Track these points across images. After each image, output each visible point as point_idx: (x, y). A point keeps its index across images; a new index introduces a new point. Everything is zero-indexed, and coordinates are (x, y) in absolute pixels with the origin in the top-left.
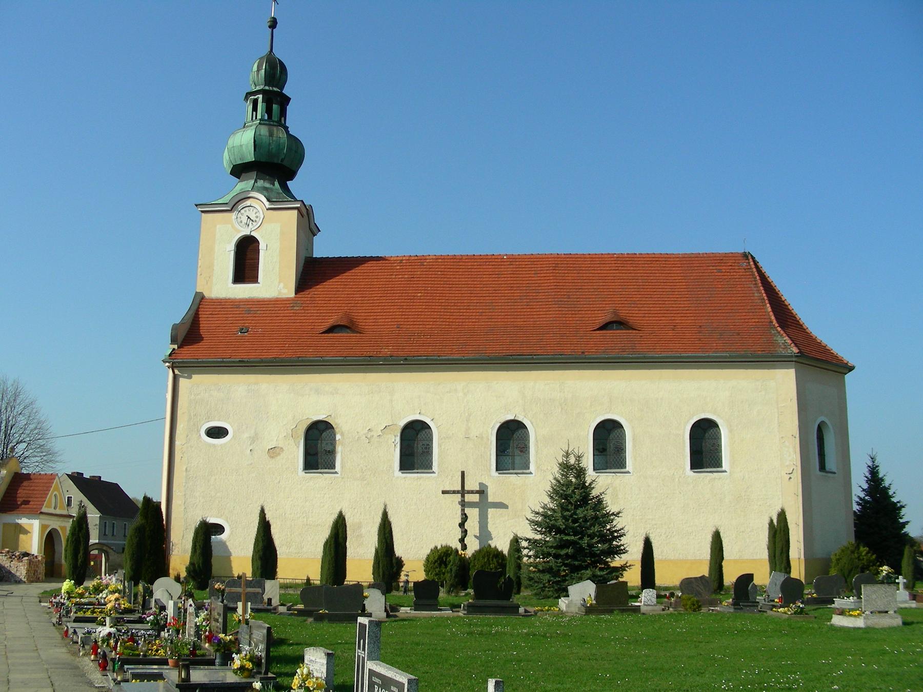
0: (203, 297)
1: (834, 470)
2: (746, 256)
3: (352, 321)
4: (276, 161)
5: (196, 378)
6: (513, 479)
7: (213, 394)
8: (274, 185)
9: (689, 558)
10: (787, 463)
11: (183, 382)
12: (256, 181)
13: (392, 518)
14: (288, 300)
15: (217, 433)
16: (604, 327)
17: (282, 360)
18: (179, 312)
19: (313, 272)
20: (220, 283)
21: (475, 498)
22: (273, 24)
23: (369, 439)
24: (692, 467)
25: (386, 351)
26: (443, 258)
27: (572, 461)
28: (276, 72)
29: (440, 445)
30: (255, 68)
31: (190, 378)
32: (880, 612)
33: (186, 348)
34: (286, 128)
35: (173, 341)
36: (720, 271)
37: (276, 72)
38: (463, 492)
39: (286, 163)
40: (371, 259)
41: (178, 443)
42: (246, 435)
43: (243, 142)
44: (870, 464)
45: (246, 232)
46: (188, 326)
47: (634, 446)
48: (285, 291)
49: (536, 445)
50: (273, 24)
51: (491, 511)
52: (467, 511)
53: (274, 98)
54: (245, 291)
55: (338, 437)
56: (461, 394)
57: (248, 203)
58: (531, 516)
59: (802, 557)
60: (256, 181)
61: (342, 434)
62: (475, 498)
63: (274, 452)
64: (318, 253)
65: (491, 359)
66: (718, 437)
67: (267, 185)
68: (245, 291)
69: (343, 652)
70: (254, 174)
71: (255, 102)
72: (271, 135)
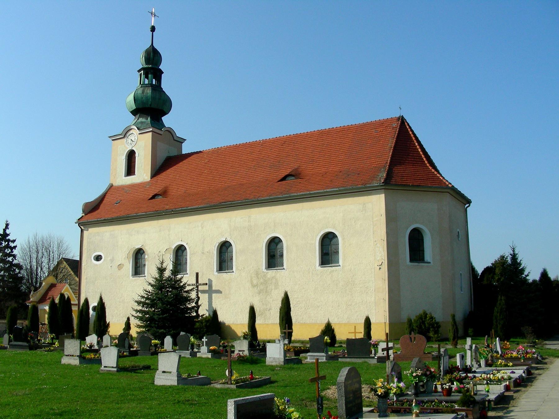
1: (429, 261)
4: (147, 106)
5: (90, 230)
6: (225, 276)
8: (147, 119)
9: (318, 322)
10: (378, 259)
11: (85, 233)
12: (138, 119)
13: (105, 300)
15: (98, 258)
17: (120, 218)
21: (206, 288)
22: (153, 29)
24: (412, 260)
29: (190, 258)
31: (88, 230)
32: (73, 356)
35: (83, 211)
39: (153, 106)
40: (197, 153)
42: (109, 258)
44: (512, 252)
45: (129, 148)
46: (97, 203)
47: (287, 252)
48: (146, 178)
49: (236, 255)
50: (153, 29)
51: (214, 295)
52: (200, 295)
56: (200, 228)
57: (131, 132)
58: (139, 299)
59: (388, 322)
60: (138, 119)
61: (148, 255)
63: (120, 266)
65: (211, 207)
69: (286, 376)
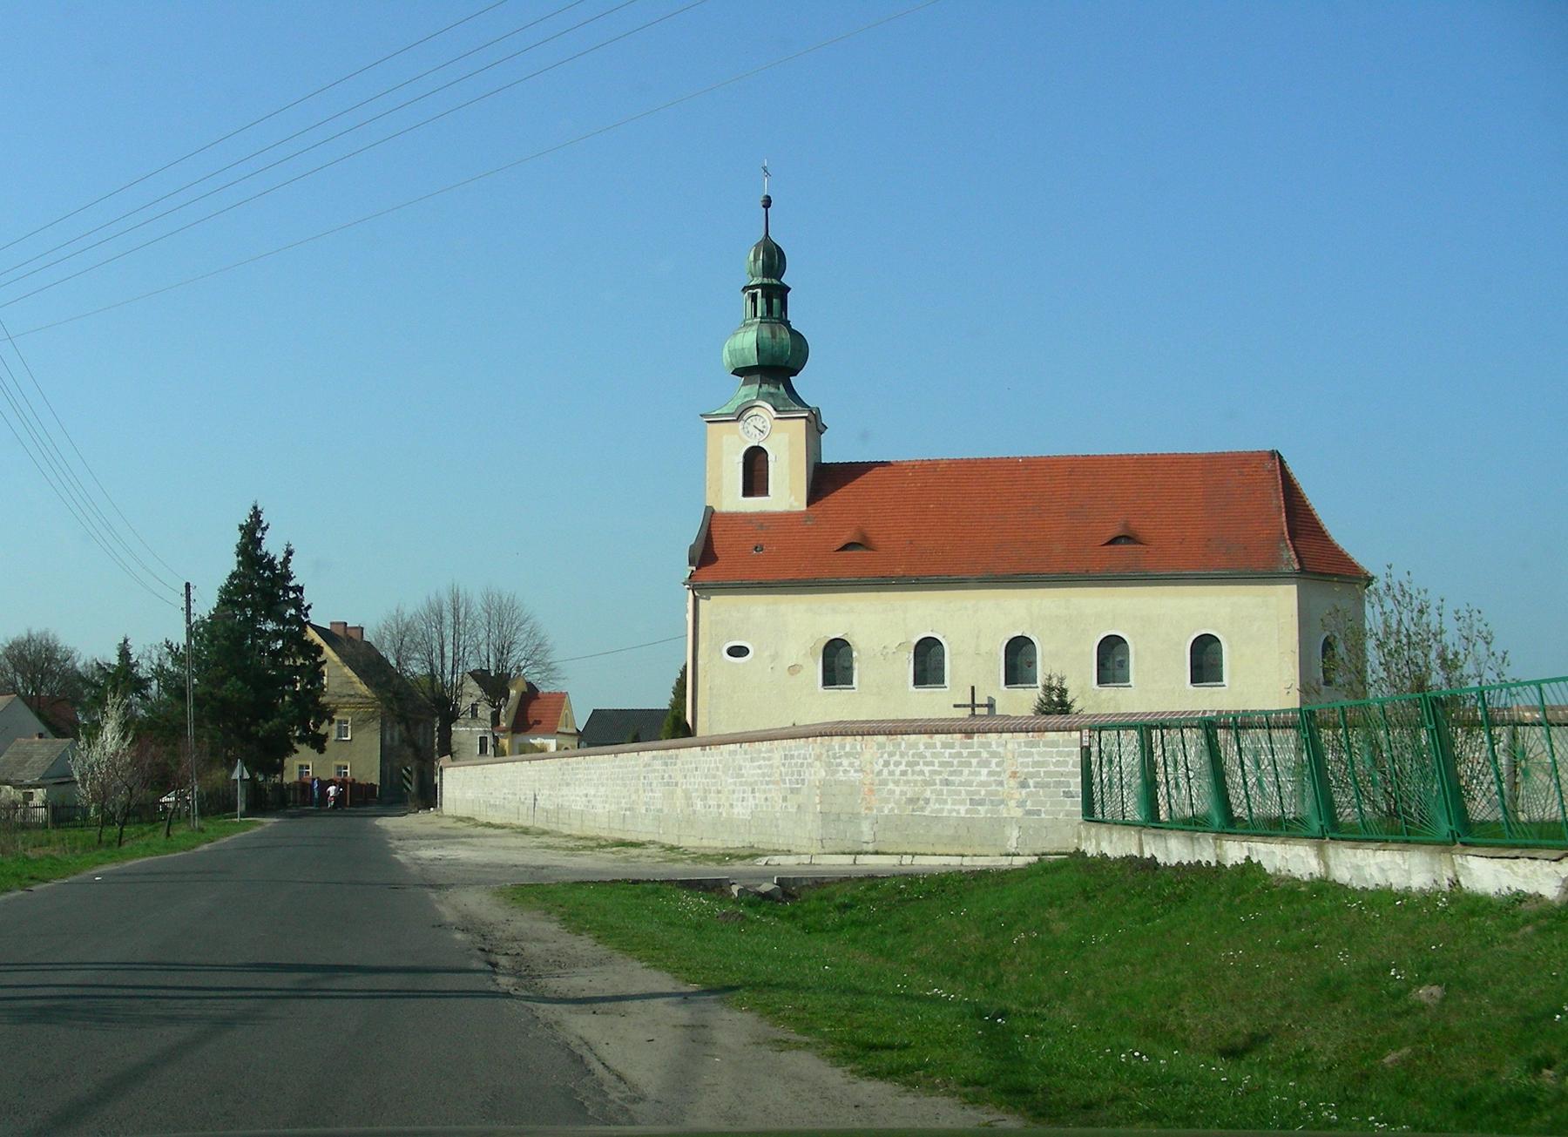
0: (713, 512)
2: (1275, 455)
3: (864, 537)
7: (729, 615)
11: (702, 602)
14: (800, 513)
15: (738, 651)
16: (1113, 541)
17: (799, 581)
18: (690, 533)
19: (825, 479)
20: (730, 498)
22: (767, 203)
23: (885, 657)
25: (899, 571)
26: (956, 462)
27: (1055, 683)
28: (773, 260)
30: (752, 257)
33: (704, 569)
34: (787, 324)
35: (691, 563)
36: (1242, 474)
37: (773, 260)
38: (973, 706)
41: (700, 662)
42: (767, 654)
43: (746, 342)
50: (767, 203)
53: (773, 295)
54: (755, 504)
55: (855, 654)
57: (754, 411)
62: (985, 711)
63: (794, 669)
64: (826, 459)
66: (1219, 653)
67: (772, 390)
68: (755, 504)
70: (758, 377)
71: (754, 297)
72: (774, 336)
